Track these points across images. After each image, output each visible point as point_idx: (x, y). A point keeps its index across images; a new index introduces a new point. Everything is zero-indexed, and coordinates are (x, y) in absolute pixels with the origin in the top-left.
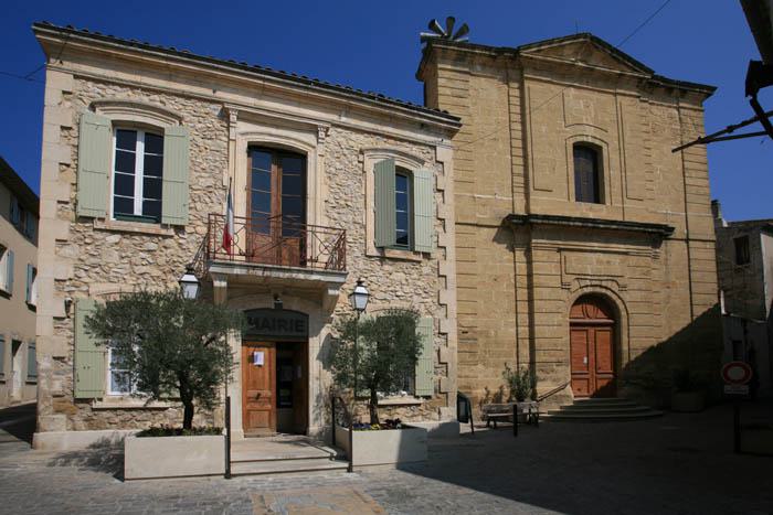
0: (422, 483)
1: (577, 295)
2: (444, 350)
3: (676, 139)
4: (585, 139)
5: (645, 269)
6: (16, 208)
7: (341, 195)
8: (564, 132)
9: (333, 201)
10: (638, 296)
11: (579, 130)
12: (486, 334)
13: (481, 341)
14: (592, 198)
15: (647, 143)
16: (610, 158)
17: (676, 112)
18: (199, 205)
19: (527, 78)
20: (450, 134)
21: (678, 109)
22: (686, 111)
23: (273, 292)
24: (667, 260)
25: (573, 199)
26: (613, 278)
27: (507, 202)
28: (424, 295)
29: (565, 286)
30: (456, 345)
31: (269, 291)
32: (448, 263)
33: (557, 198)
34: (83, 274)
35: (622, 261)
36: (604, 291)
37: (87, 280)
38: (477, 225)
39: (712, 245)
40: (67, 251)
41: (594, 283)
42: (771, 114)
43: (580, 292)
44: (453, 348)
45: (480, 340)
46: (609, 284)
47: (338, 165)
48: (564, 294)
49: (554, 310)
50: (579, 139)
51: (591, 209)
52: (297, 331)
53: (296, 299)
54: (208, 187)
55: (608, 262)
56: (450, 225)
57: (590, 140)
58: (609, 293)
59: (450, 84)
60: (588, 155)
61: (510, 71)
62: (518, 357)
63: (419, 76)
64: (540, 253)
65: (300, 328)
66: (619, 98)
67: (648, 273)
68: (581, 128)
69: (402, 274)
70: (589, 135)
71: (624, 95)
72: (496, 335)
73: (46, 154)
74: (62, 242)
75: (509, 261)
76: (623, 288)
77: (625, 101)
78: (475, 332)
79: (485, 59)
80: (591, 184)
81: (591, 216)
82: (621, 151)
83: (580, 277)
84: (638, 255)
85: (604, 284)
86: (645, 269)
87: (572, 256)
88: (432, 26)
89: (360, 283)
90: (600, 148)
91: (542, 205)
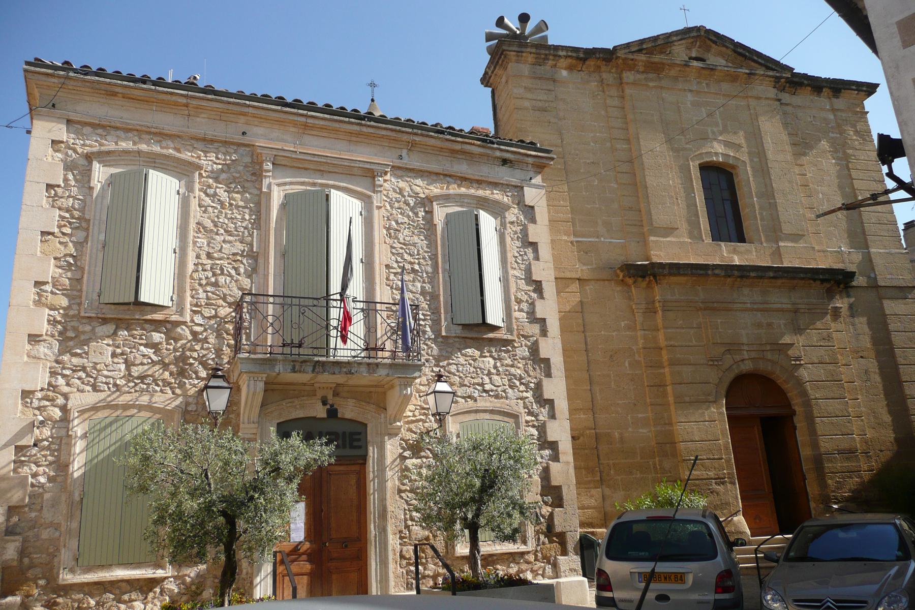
2: (554, 467)
5: (825, 333)
6: (904, 301)
7: (406, 256)
9: (395, 265)
10: (820, 372)
14: (733, 233)
17: (832, 117)
18: (222, 280)
20: (540, 168)
21: (833, 110)
23: (320, 394)
27: (617, 248)
28: (522, 388)
30: (571, 458)
31: (313, 394)
32: (549, 340)
33: (683, 241)
34: (61, 381)
37: (66, 389)
39: (819, 433)
40: (42, 349)
42: (902, 292)
44: (568, 463)
47: (401, 218)
50: (707, 159)
51: (735, 251)
52: (352, 447)
53: (351, 402)
54: (234, 254)
55: (770, 325)
56: (549, 289)
59: (529, 96)
60: (720, 181)
61: (604, 75)
63: (486, 81)
65: (356, 444)
69: (491, 360)
72: (622, 439)
73: (25, 220)
74: (34, 339)
79: (569, 60)
80: (728, 221)
82: (763, 170)
88: (500, 22)
89: (439, 378)
91: (664, 251)
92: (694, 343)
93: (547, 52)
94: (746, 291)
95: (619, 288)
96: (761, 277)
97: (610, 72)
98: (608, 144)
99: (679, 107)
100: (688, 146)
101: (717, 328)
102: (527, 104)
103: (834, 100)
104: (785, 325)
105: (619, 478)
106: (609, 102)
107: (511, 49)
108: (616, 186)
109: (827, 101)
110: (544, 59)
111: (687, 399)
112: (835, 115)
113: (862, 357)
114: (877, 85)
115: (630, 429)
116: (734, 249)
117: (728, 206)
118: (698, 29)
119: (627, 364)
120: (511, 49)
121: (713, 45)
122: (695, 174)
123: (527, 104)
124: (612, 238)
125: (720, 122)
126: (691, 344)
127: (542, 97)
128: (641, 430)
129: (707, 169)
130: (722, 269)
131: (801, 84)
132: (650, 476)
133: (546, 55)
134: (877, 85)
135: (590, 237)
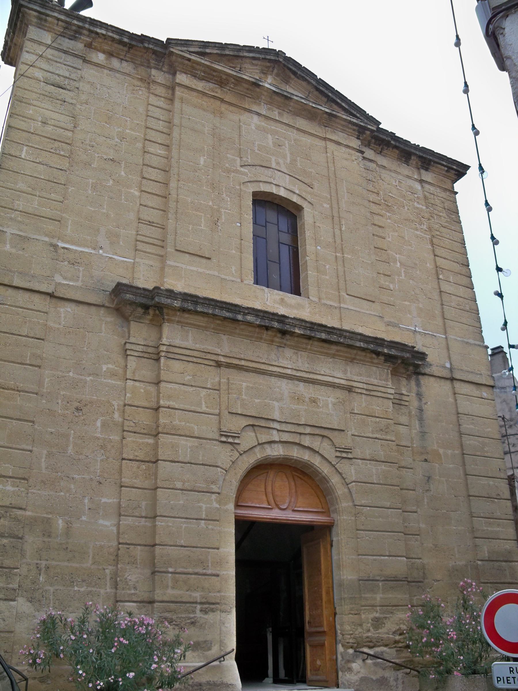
0: (317, 242)
1: (250, 460)
3: (421, 223)
4: (274, 190)
8: (237, 171)
10: (375, 471)
11: (263, 175)
12: (46, 528)
13: (32, 541)
15: (376, 217)
16: (313, 222)
19: (180, 85)
21: (421, 181)
22: (432, 189)
24: (421, 410)
25: (250, 279)
26: (323, 432)
29: (228, 439)
35: (353, 409)
36: (306, 456)
38: (51, 295)
41: (286, 437)
43: (258, 455)
45: (29, 538)
46: (316, 443)
48: (223, 455)
49: (202, 486)
57: (282, 193)
58: (316, 461)
60: (276, 213)
62: (309, 202)
64: (177, 366)
66: (331, 146)
67: (385, 430)
68: (269, 172)
70: (282, 187)
71: (338, 143)
72: (68, 531)
75: (113, 374)
76: (345, 453)
77: (341, 152)
78: (16, 519)
81: (282, 311)
83: (258, 422)
84: (369, 393)
85: (307, 441)
86: (384, 422)
87: (243, 382)
90: (299, 208)
91: (185, 278)
92: (204, 409)
93: (81, 24)
94: (289, 352)
95: (109, 319)
96: (310, 338)
97: (161, 70)
98: (139, 145)
99: (240, 127)
100: (242, 169)
101: (240, 394)
102: (39, 74)
103: (423, 171)
104: (334, 404)
105: (52, 589)
106: (153, 99)
107: (31, 6)
108: (137, 193)
109: (415, 170)
110: (76, 32)
111: (179, 485)
112: (422, 187)
113: (426, 460)
114: (467, 167)
115: (84, 518)
116: (282, 300)
117: (285, 251)
118: (280, 54)
119: (99, 424)
120: (31, 6)
121: (293, 76)
122: (249, 202)
123: (39, 74)
124: (116, 254)
125: (288, 155)
126: (199, 410)
127: (64, 71)
128: (101, 522)
129: (263, 201)
130: (257, 316)
131: (388, 144)
132: (102, 591)
133: (79, 27)
134: (467, 167)
135: (84, 246)
